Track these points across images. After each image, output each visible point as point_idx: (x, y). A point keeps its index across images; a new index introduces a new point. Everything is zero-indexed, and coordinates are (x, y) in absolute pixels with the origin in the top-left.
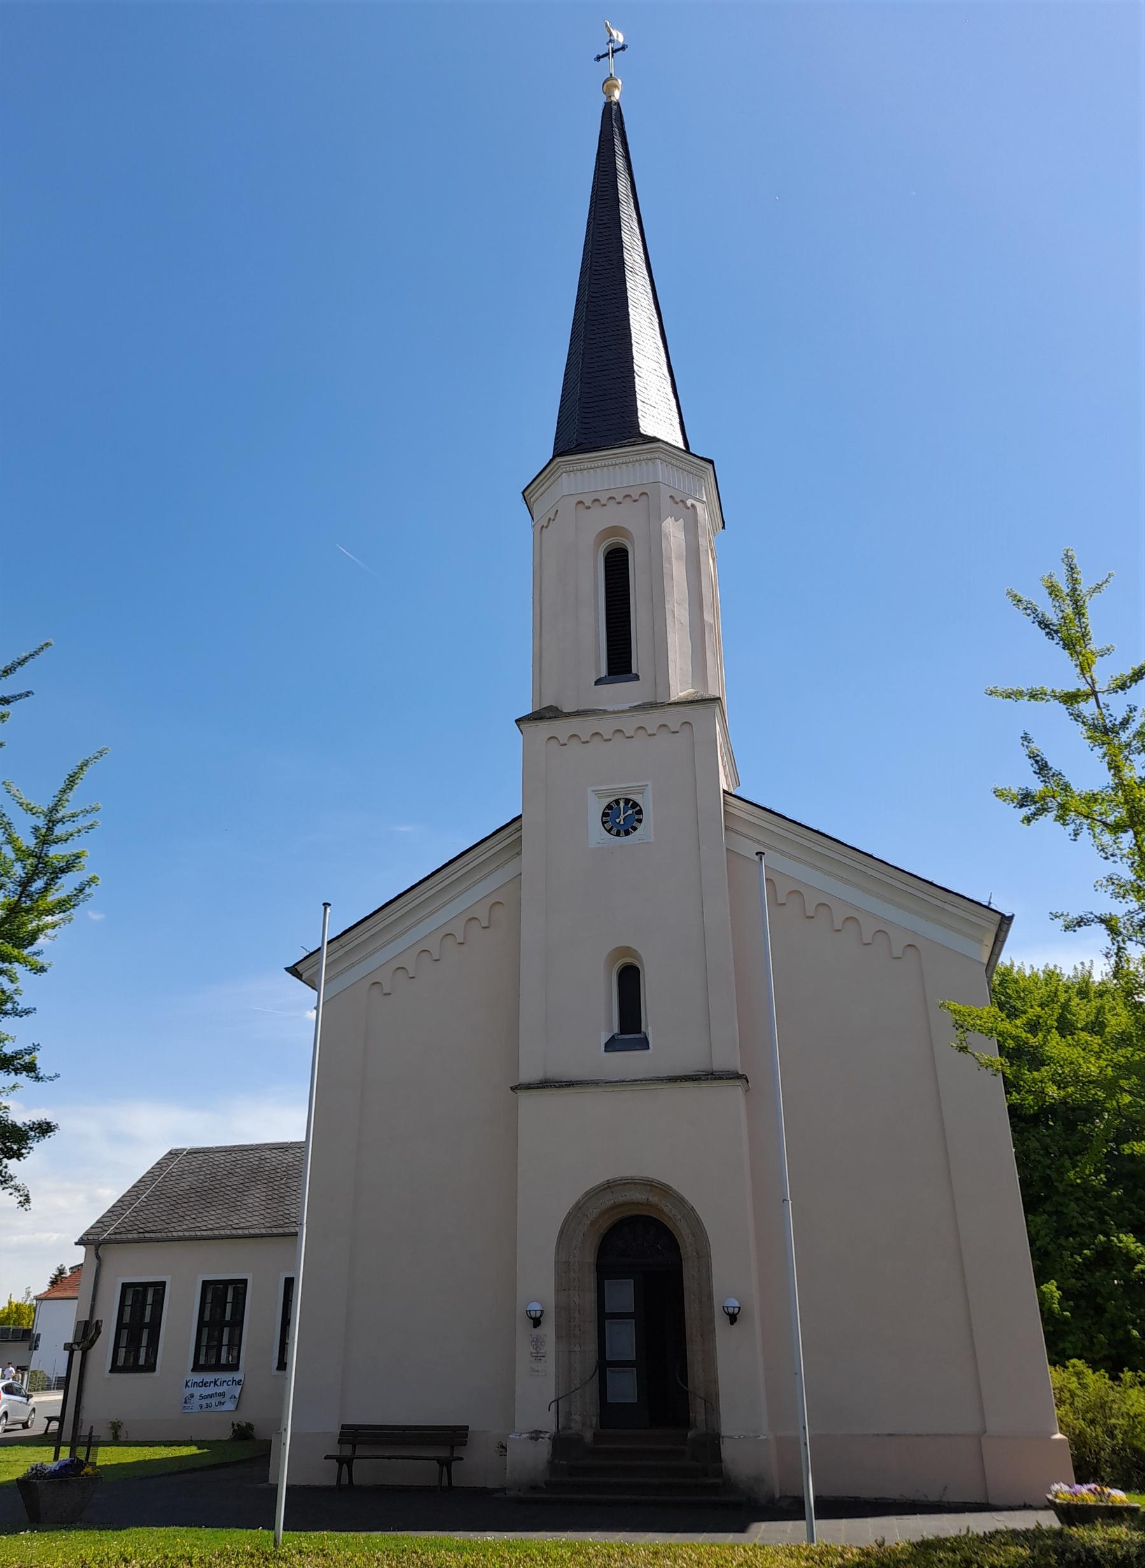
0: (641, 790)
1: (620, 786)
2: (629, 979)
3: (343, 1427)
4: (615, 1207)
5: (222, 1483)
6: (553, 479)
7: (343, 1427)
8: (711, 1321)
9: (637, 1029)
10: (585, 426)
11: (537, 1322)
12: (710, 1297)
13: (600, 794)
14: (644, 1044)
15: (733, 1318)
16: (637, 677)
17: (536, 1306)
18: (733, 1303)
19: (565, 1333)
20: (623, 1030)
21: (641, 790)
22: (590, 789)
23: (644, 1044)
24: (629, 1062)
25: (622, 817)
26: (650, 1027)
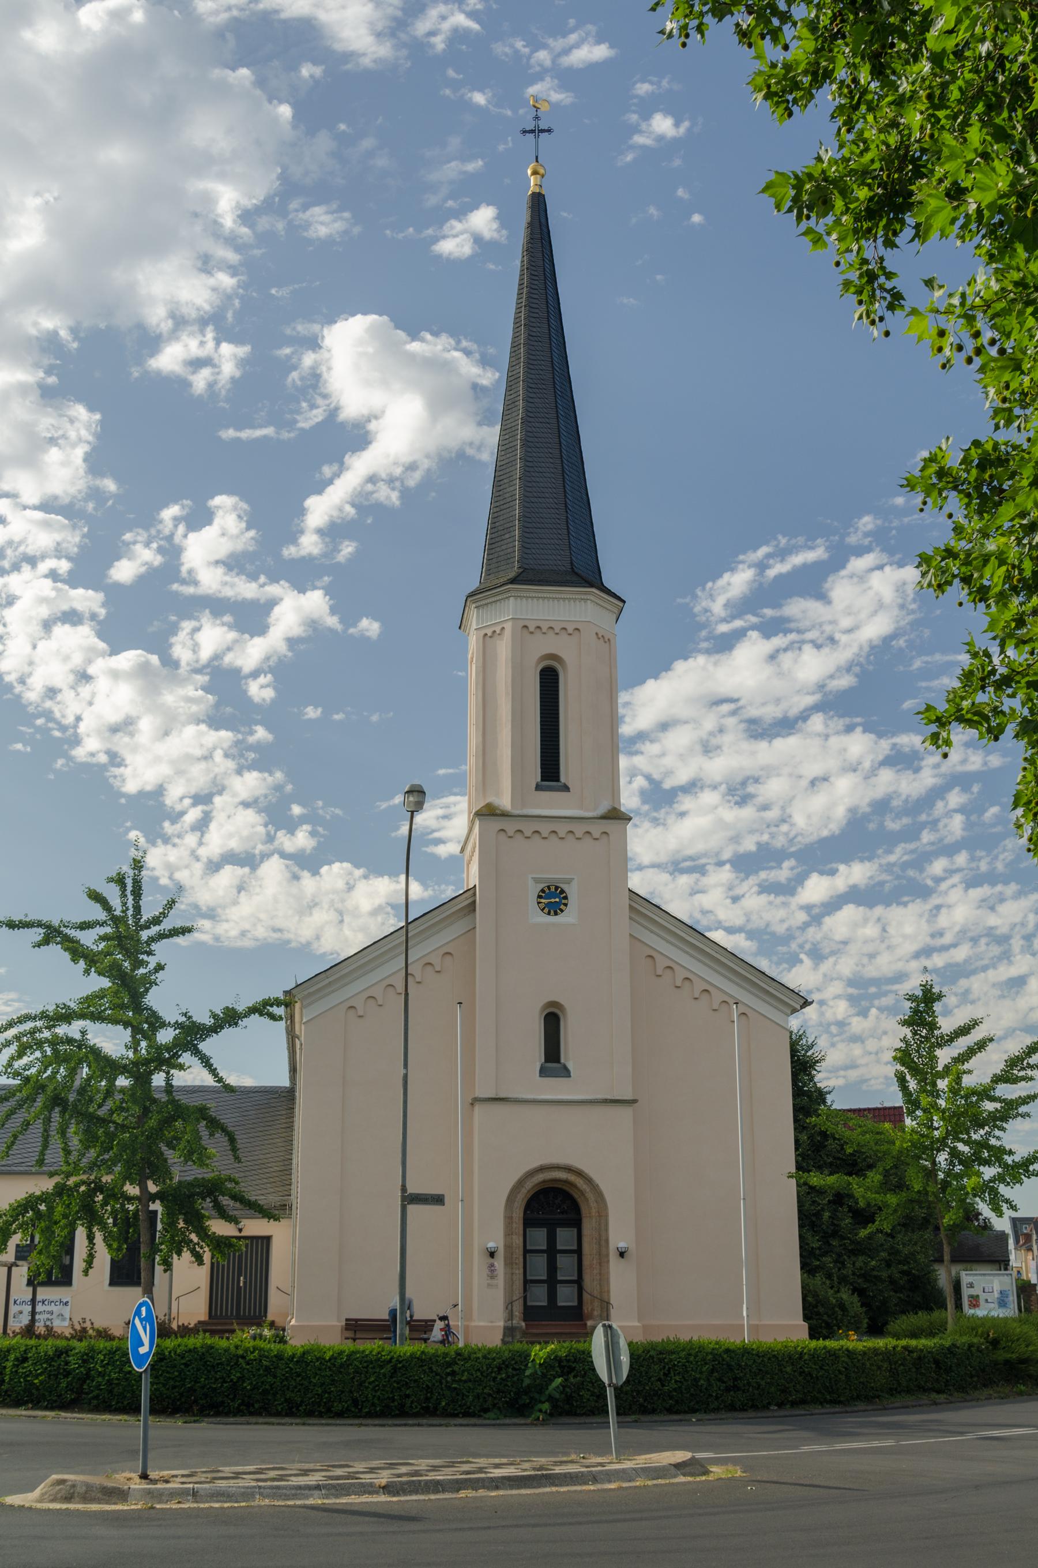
0: (569, 881)
1: (553, 875)
2: (552, 1021)
3: (347, 1320)
4: (544, 1181)
5: (223, 1382)
6: (498, 598)
7: (347, 1320)
8: (608, 1255)
9: (557, 1060)
10: (526, 556)
11: (492, 1255)
12: (607, 1241)
13: (537, 880)
14: (566, 1072)
15: (622, 1254)
16: (566, 788)
17: (491, 1245)
18: (622, 1245)
19: (509, 1263)
20: (547, 1060)
21: (569, 881)
22: (530, 876)
23: (566, 1072)
24: (555, 1089)
25: (553, 898)
26: (570, 1055)
